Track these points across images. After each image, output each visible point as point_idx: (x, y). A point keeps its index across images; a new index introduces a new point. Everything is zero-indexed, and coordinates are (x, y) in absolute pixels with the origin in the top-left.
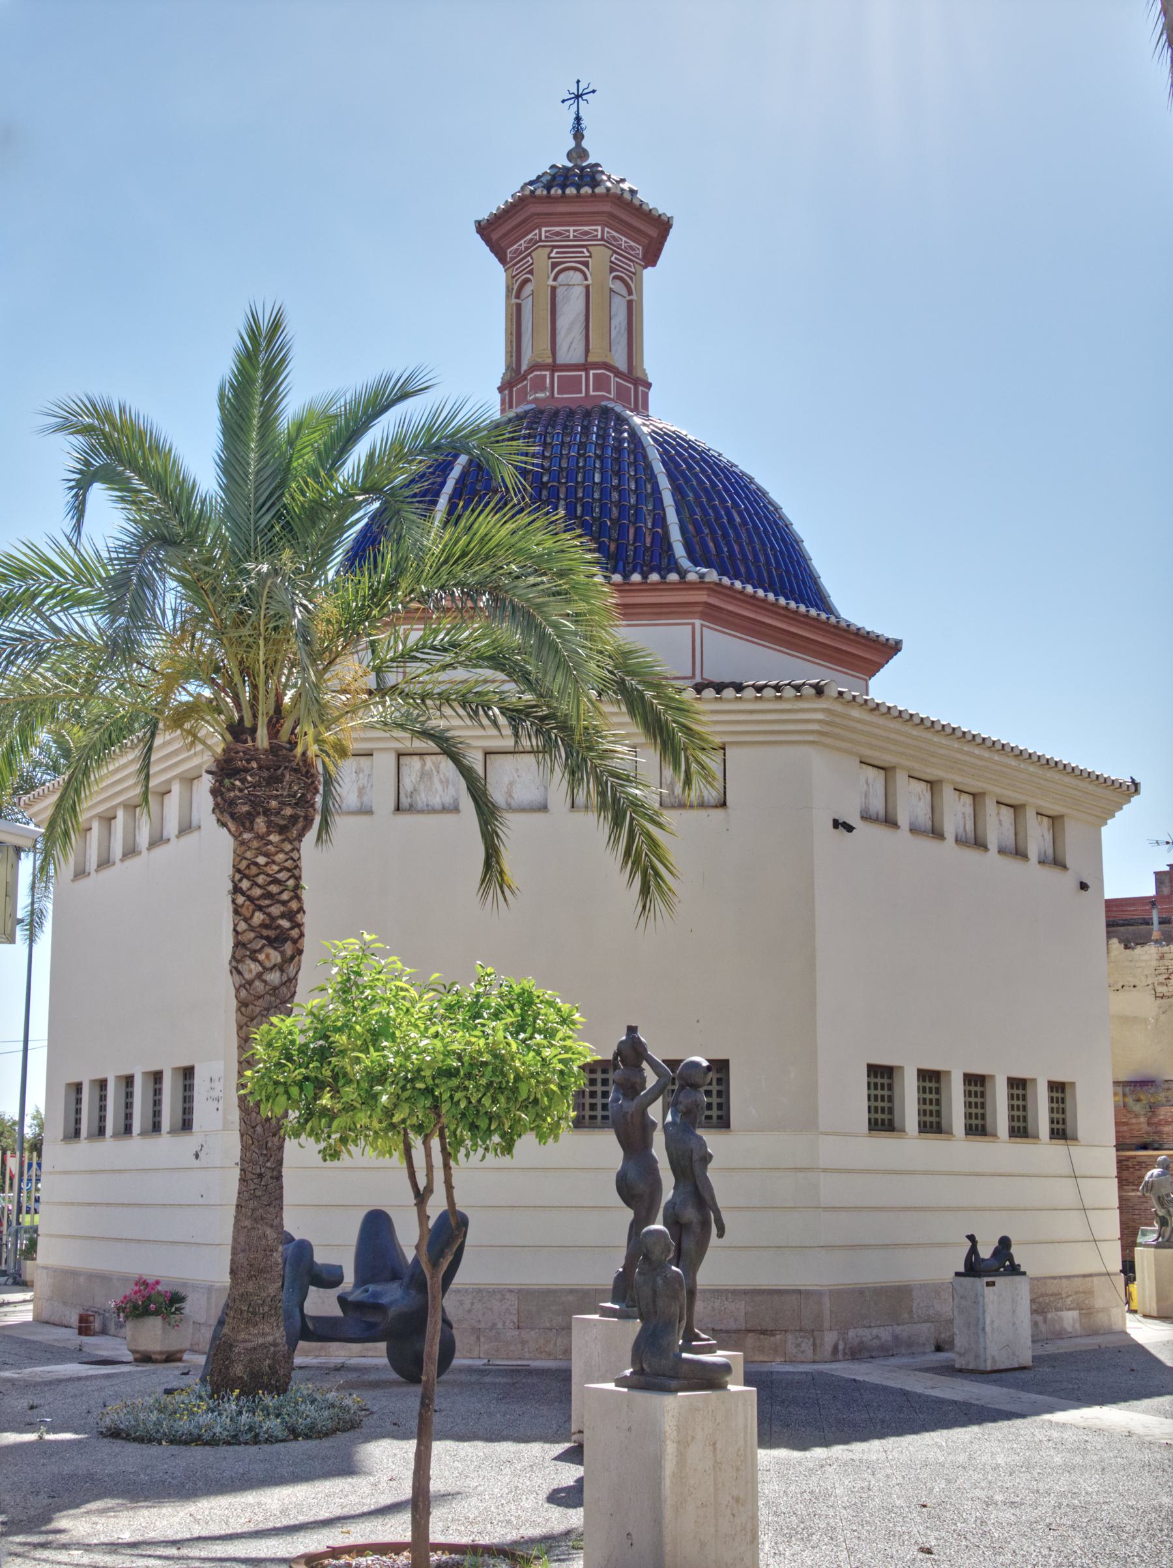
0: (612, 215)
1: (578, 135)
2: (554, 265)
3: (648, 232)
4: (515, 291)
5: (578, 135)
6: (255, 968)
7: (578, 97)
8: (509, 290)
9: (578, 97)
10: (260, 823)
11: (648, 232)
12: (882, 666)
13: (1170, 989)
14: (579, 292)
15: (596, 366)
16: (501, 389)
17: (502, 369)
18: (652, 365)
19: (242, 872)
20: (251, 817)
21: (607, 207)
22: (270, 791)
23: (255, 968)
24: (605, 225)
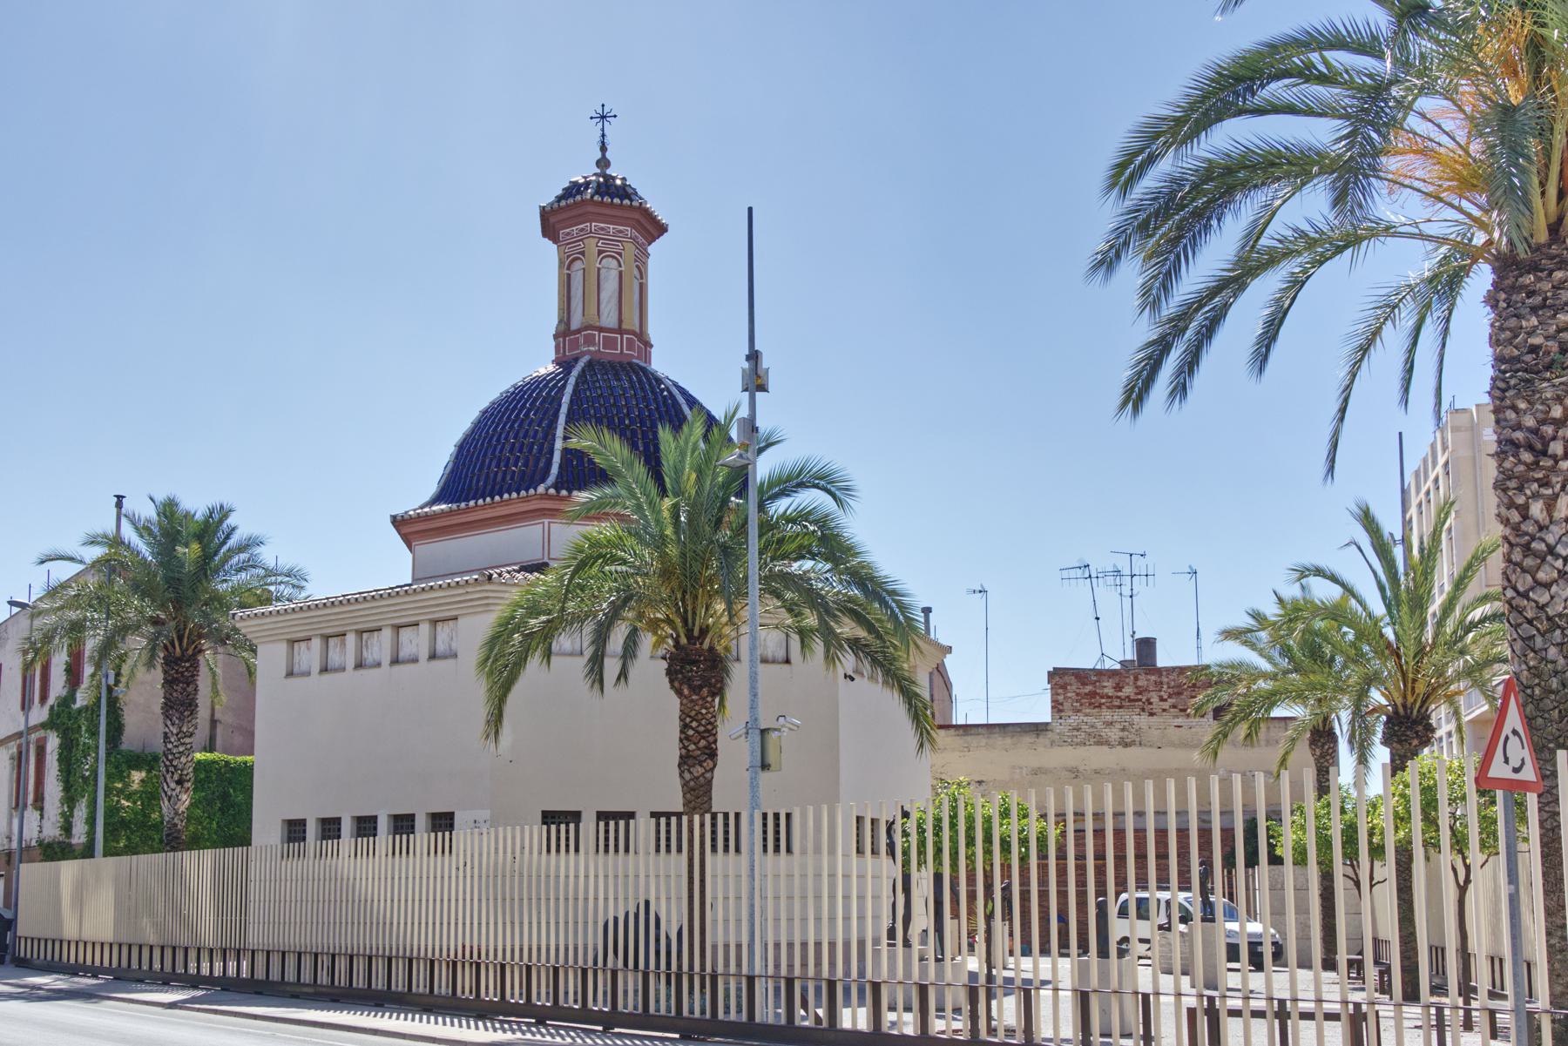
0: (638, 221)
1: (603, 148)
2: (600, 252)
3: (653, 228)
4: (566, 264)
5: (603, 148)
6: (701, 770)
7: (603, 117)
8: (561, 263)
9: (603, 117)
10: (705, 690)
11: (653, 228)
12: (1559, 826)
13: (1513, 3)
14: (614, 274)
15: (628, 332)
16: (556, 337)
17: (555, 322)
18: (654, 332)
19: (684, 714)
20: (701, 687)
21: (637, 216)
22: (698, 671)
23: (701, 770)
24: (633, 227)
